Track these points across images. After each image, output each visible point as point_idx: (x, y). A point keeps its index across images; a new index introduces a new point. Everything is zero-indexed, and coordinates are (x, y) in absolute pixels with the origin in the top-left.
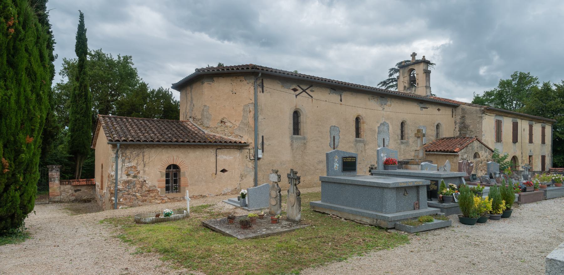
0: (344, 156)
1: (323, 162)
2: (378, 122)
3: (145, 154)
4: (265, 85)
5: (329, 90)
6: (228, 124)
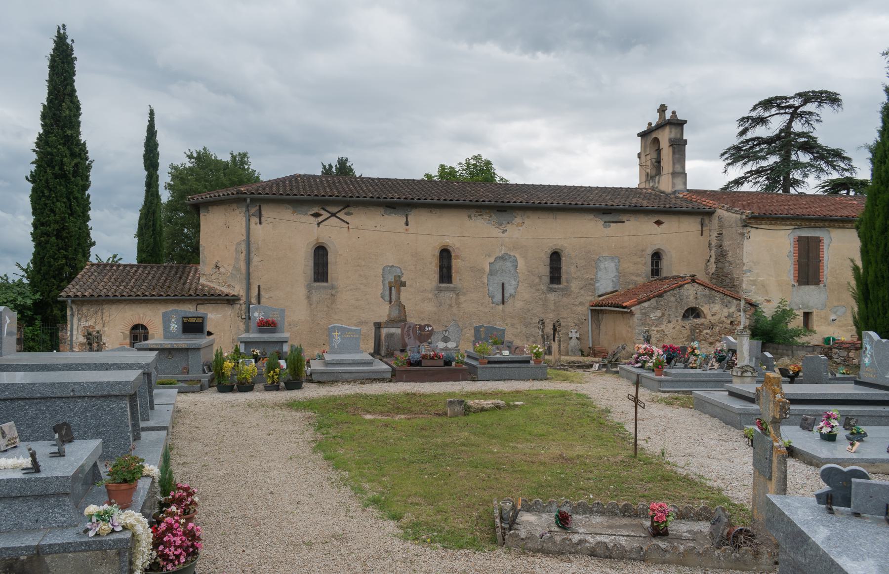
0: (185, 316)
1: (367, 323)
2: (489, 256)
3: (104, 311)
4: (263, 213)
5: (382, 210)
6: (222, 270)
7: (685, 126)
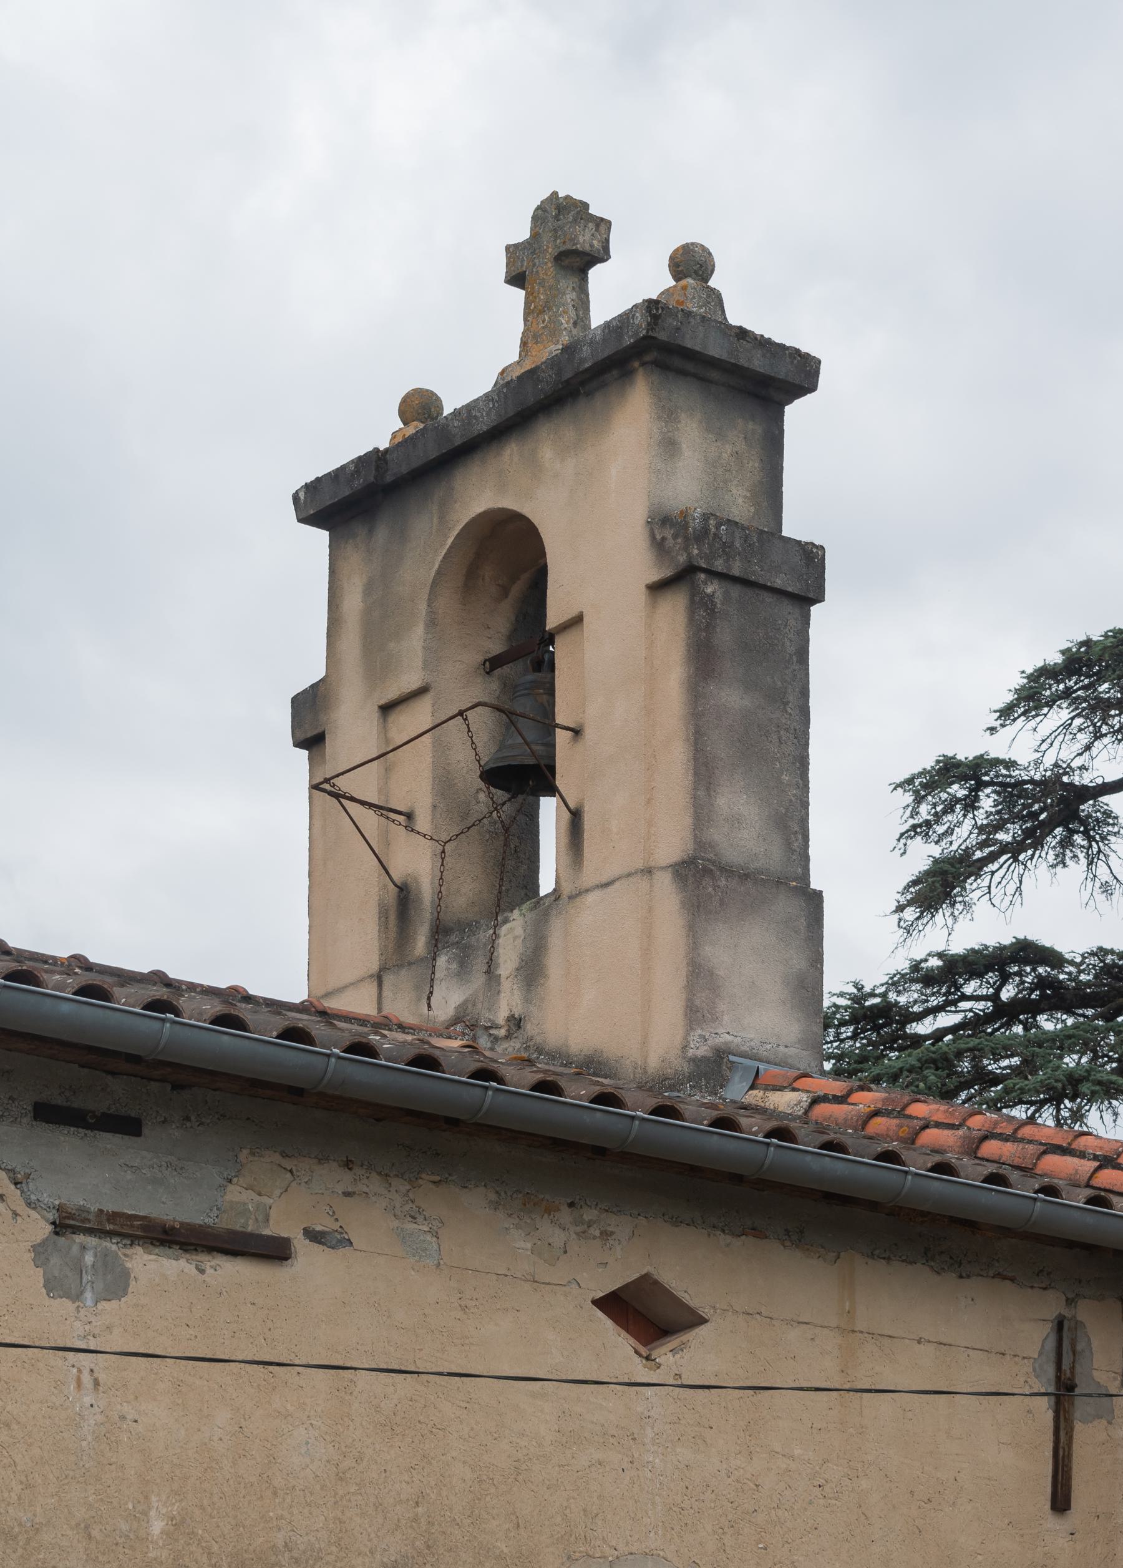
7: (795, 413)
